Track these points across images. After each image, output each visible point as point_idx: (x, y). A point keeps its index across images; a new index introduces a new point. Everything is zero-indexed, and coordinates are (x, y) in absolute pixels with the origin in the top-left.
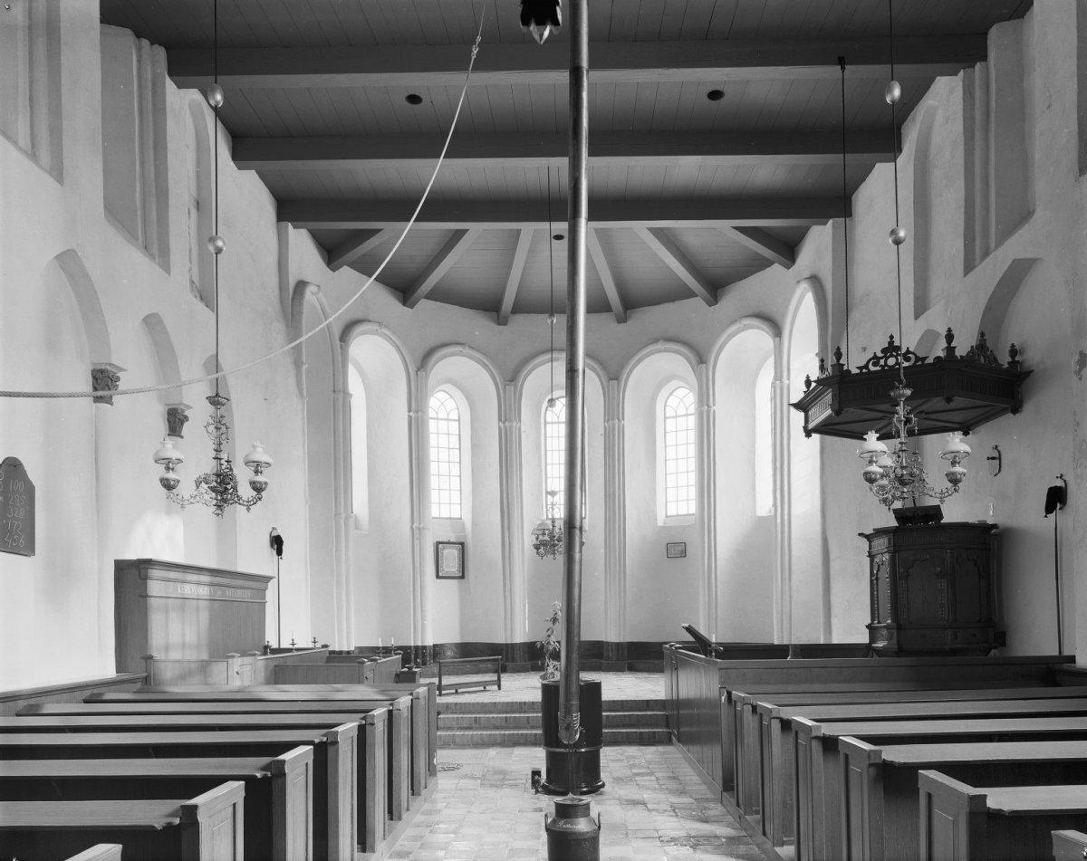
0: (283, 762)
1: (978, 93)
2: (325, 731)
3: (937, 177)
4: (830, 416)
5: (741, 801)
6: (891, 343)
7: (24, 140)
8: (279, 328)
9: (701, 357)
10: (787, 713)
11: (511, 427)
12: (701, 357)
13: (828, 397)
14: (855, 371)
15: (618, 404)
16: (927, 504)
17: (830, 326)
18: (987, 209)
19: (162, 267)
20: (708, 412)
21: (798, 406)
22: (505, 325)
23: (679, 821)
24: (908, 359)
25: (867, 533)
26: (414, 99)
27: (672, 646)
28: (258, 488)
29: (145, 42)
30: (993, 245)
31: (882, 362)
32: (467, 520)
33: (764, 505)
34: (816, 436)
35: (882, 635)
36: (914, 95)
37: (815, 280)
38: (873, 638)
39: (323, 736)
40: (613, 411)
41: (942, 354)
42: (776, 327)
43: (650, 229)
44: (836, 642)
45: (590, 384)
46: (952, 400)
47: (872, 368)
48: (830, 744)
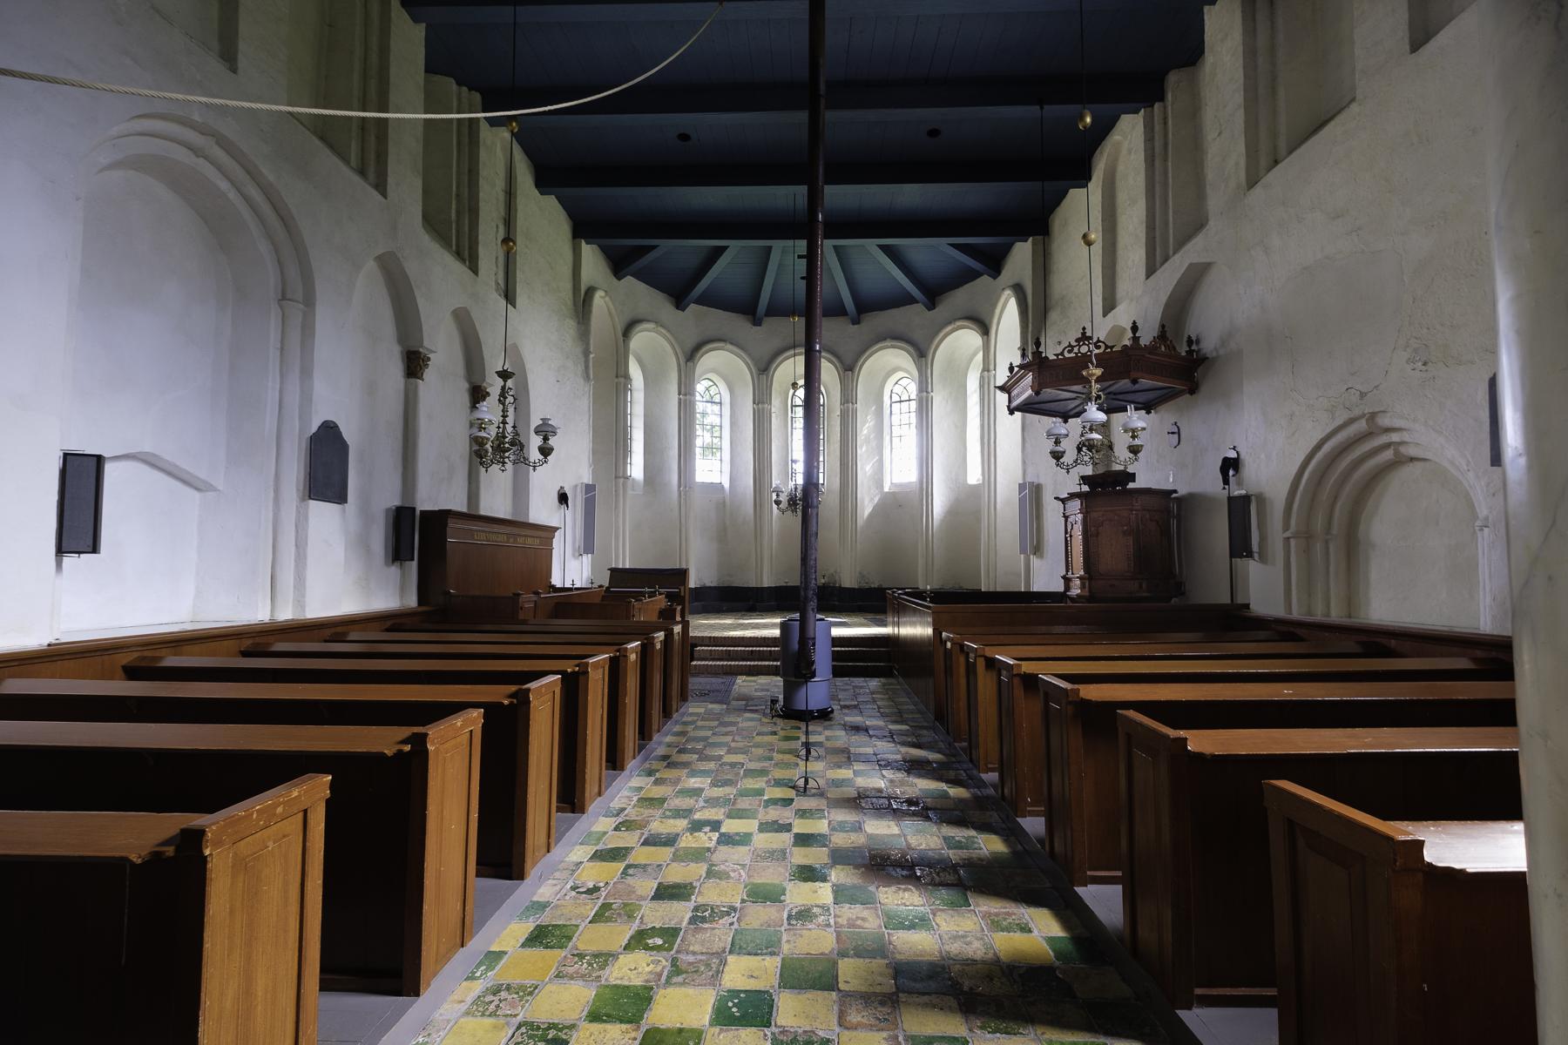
0: (528, 690)
1: (1158, 128)
2: (577, 662)
3: (1122, 197)
4: (1030, 396)
5: (950, 731)
6: (1084, 334)
7: (354, 159)
8: (570, 325)
9: (922, 353)
10: (989, 652)
11: (763, 409)
12: (922, 353)
13: (1029, 378)
14: (1052, 357)
15: (852, 391)
16: (1114, 469)
17: (1030, 325)
18: (1166, 224)
19: (470, 269)
20: (927, 398)
21: (1002, 388)
22: (760, 325)
23: (896, 747)
24: (1098, 347)
25: (1062, 497)
26: (684, 137)
27: (894, 592)
28: (546, 451)
29: (465, 89)
30: (1171, 253)
31: (1076, 350)
32: (727, 485)
33: (974, 476)
34: (1018, 415)
35: (1075, 585)
36: (1103, 129)
37: (1018, 290)
38: (1067, 588)
39: (576, 666)
40: (848, 397)
41: (1128, 343)
42: (985, 329)
43: (879, 246)
44: (1035, 590)
45: (828, 372)
46: (1137, 382)
47: (1067, 355)
48: (1031, 681)
